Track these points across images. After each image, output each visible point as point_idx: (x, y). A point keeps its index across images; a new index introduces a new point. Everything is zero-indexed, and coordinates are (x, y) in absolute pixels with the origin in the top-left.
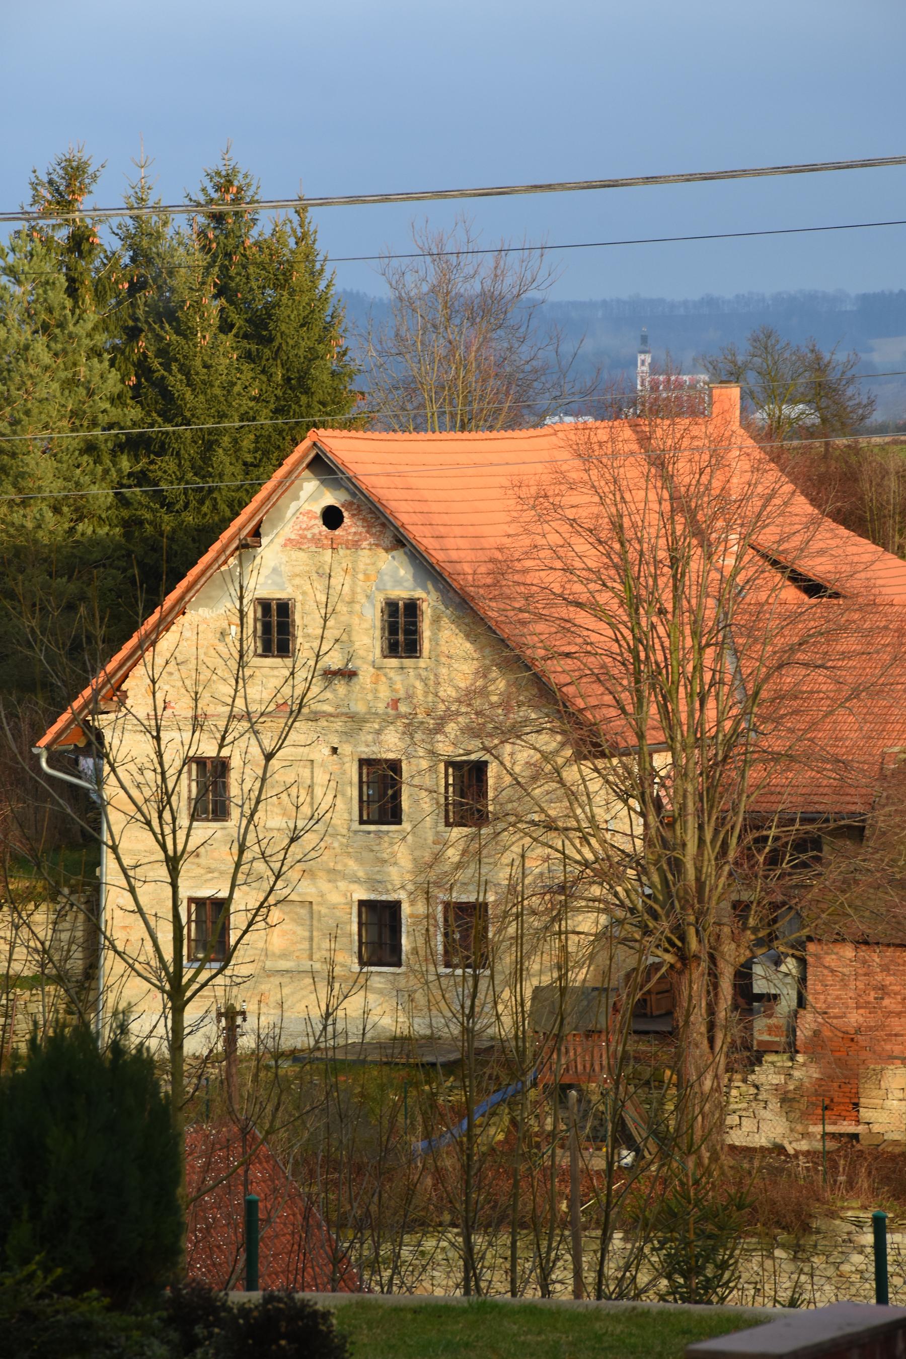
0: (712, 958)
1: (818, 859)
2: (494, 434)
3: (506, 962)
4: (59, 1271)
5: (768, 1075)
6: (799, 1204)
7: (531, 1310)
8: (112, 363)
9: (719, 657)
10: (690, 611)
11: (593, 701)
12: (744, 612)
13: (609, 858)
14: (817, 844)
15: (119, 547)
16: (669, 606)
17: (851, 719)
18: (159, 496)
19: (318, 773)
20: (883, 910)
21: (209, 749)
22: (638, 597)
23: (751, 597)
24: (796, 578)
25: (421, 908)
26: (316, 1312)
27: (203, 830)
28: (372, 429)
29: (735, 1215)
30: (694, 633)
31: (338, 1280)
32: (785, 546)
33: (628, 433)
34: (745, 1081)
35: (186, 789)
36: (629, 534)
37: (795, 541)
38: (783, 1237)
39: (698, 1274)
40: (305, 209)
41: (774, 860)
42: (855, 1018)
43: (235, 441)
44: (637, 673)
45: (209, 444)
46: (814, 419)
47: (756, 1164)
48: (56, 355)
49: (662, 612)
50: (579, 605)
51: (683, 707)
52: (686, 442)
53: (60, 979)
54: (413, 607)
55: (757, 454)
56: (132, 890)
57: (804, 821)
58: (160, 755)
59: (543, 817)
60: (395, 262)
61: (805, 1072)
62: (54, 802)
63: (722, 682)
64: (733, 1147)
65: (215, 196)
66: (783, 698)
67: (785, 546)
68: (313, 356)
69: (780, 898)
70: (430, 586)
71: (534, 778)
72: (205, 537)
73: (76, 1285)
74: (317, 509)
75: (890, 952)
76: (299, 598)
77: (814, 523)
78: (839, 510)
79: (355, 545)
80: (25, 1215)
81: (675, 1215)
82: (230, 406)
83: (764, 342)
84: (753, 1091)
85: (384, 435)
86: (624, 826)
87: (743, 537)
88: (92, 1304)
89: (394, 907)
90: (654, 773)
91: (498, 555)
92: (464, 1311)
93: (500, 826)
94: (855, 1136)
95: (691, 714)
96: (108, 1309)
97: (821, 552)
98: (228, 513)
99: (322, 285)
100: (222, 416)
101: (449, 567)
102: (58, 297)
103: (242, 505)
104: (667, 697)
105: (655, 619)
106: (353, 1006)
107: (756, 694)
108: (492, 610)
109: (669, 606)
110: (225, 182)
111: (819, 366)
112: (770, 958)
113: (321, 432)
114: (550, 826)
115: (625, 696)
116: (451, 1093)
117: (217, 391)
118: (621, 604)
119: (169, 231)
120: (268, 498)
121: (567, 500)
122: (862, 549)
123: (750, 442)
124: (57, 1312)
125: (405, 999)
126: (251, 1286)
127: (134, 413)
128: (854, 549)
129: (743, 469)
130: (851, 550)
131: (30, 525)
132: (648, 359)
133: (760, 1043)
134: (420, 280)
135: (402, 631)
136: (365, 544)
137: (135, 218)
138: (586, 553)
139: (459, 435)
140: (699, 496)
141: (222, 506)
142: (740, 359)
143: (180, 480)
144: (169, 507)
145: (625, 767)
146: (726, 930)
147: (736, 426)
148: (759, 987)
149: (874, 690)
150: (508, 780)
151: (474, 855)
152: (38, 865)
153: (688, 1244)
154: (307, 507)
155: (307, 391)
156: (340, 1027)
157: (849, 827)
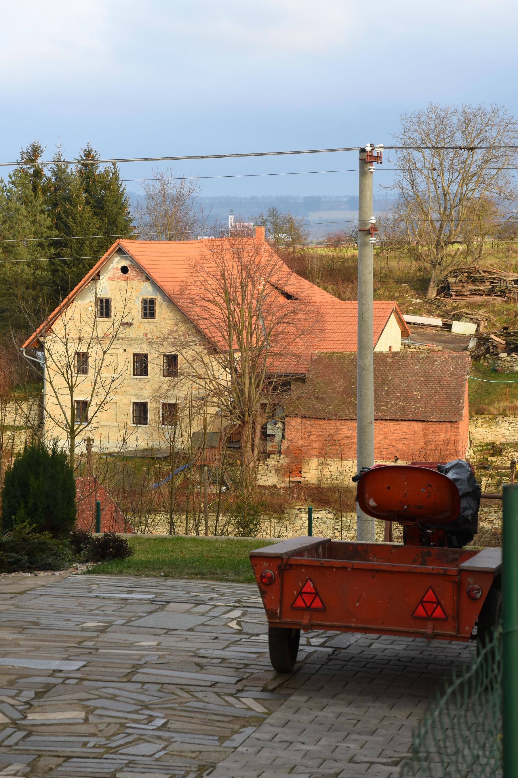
0: (254, 422)
1: (289, 389)
2: (181, 242)
3: (185, 422)
4: (35, 525)
5: (272, 462)
6: (281, 504)
7: (194, 540)
8: (48, 216)
9: (257, 320)
10: (248, 304)
11: (214, 335)
12: (266, 304)
13: (219, 388)
14: (289, 384)
15: (50, 279)
16: (240, 302)
17: (301, 341)
18: (64, 262)
19: (122, 359)
20: (311, 406)
21: (84, 349)
22: (230, 299)
23: (268, 300)
24: (284, 293)
25: (155, 405)
26: (122, 540)
27: (82, 377)
28: (175, 240)
29: (261, 508)
30: (249, 312)
31: (127, 529)
32: (280, 282)
33: (227, 242)
34: (264, 463)
35: (74, 363)
36: (227, 277)
37: (283, 281)
38: (275, 515)
39: (247, 527)
40: (115, 163)
41: (275, 389)
42: (301, 442)
43: (91, 243)
44: (230, 325)
45: (81, 243)
46: (289, 239)
47: (267, 491)
48: (29, 212)
49: (238, 304)
50: (209, 301)
51: (245, 337)
52: (246, 246)
53: (32, 427)
54: (152, 302)
55: (270, 250)
56: (57, 397)
57: (285, 376)
58: (67, 351)
59: (196, 374)
60: (146, 182)
61: (284, 461)
62: (30, 367)
63: (258, 329)
64: (259, 486)
65: (84, 158)
66: (279, 334)
67: (280, 282)
68: (118, 214)
69: (276, 402)
70: (158, 294)
71: (194, 361)
72: (80, 277)
73: (40, 530)
74: (120, 267)
75: (313, 421)
76: (113, 297)
77: (290, 274)
78: (298, 270)
79: (132, 279)
80: (22, 506)
81: (240, 508)
82: (89, 230)
83: (273, 212)
84: (266, 467)
85: (142, 242)
86: (224, 377)
87: (266, 279)
88: (46, 536)
89: (145, 405)
90: (235, 359)
91: (181, 284)
92: (171, 540)
93: (182, 377)
94: (300, 482)
95: (247, 339)
96: (51, 538)
97: (292, 284)
98: (88, 267)
99: (121, 190)
100: (86, 234)
101: (165, 288)
102: (30, 192)
103: (93, 265)
104: (240, 333)
105: (235, 307)
106: (133, 438)
107: (270, 333)
108: (180, 302)
109: (240, 302)
110: (88, 154)
111: (290, 221)
112: (273, 422)
113: (121, 240)
114: (199, 377)
115: (225, 333)
116: (166, 467)
117: (85, 226)
118: (224, 301)
119: (68, 170)
120: (102, 263)
121: (205, 265)
122: (306, 283)
123: (268, 247)
124: (34, 539)
125: (150, 435)
126: (98, 530)
127: (56, 232)
128: (303, 284)
129: (266, 256)
130: (302, 284)
131: (19, 271)
132: (233, 217)
133: (269, 451)
134: (155, 188)
135: (149, 309)
136: (136, 279)
137: (57, 165)
138: (213, 284)
139: (168, 242)
140: (250, 265)
141: (86, 266)
142: (265, 218)
143: (72, 256)
144: (68, 265)
145: (225, 357)
146: (259, 413)
147: (263, 241)
148: (269, 432)
149: (309, 332)
150: (185, 361)
151: (171, 387)
152: (25, 388)
153: (245, 518)
154: (116, 266)
155: (116, 226)
156: (128, 445)
157: (300, 378)
